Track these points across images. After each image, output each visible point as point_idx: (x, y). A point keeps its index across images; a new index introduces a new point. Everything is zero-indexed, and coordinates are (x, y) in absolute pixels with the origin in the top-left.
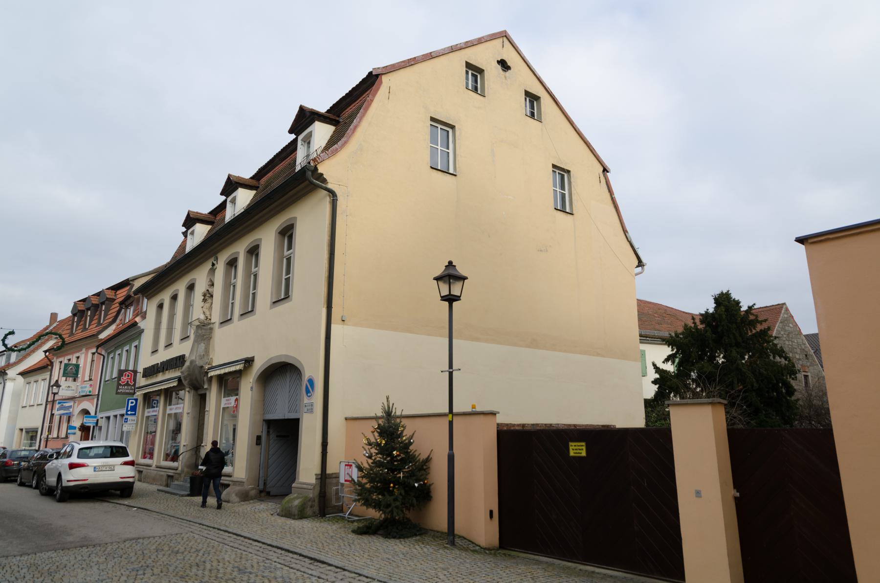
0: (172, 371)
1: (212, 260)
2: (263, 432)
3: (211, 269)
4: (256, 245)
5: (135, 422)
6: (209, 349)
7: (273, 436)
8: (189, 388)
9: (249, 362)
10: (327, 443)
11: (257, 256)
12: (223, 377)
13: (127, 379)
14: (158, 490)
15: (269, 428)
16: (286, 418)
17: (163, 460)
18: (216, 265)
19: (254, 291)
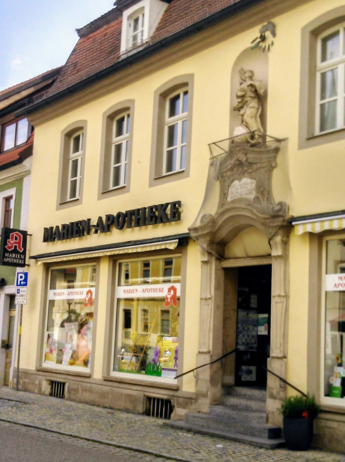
13: (15, 243)
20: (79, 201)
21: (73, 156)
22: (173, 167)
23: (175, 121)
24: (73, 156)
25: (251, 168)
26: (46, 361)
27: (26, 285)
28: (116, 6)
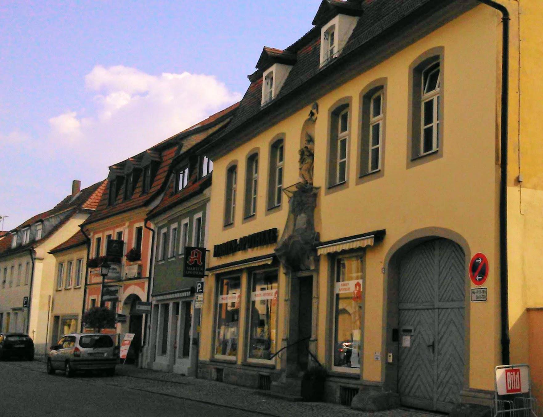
0: (257, 249)
1: (308, 109)
3: (308, 120)
9: (379, 236)
11: (282, 149)
13: (195, 258)
17: (180, 357)
18: (316, 115)
19: (343, 160)
20: (439, 153)
21: (374, 120)
23: (431, 97)
24: (426, 96)
25: (124, 266)
26: (218, 354)
27: (202, 292)
28: (258, 69)
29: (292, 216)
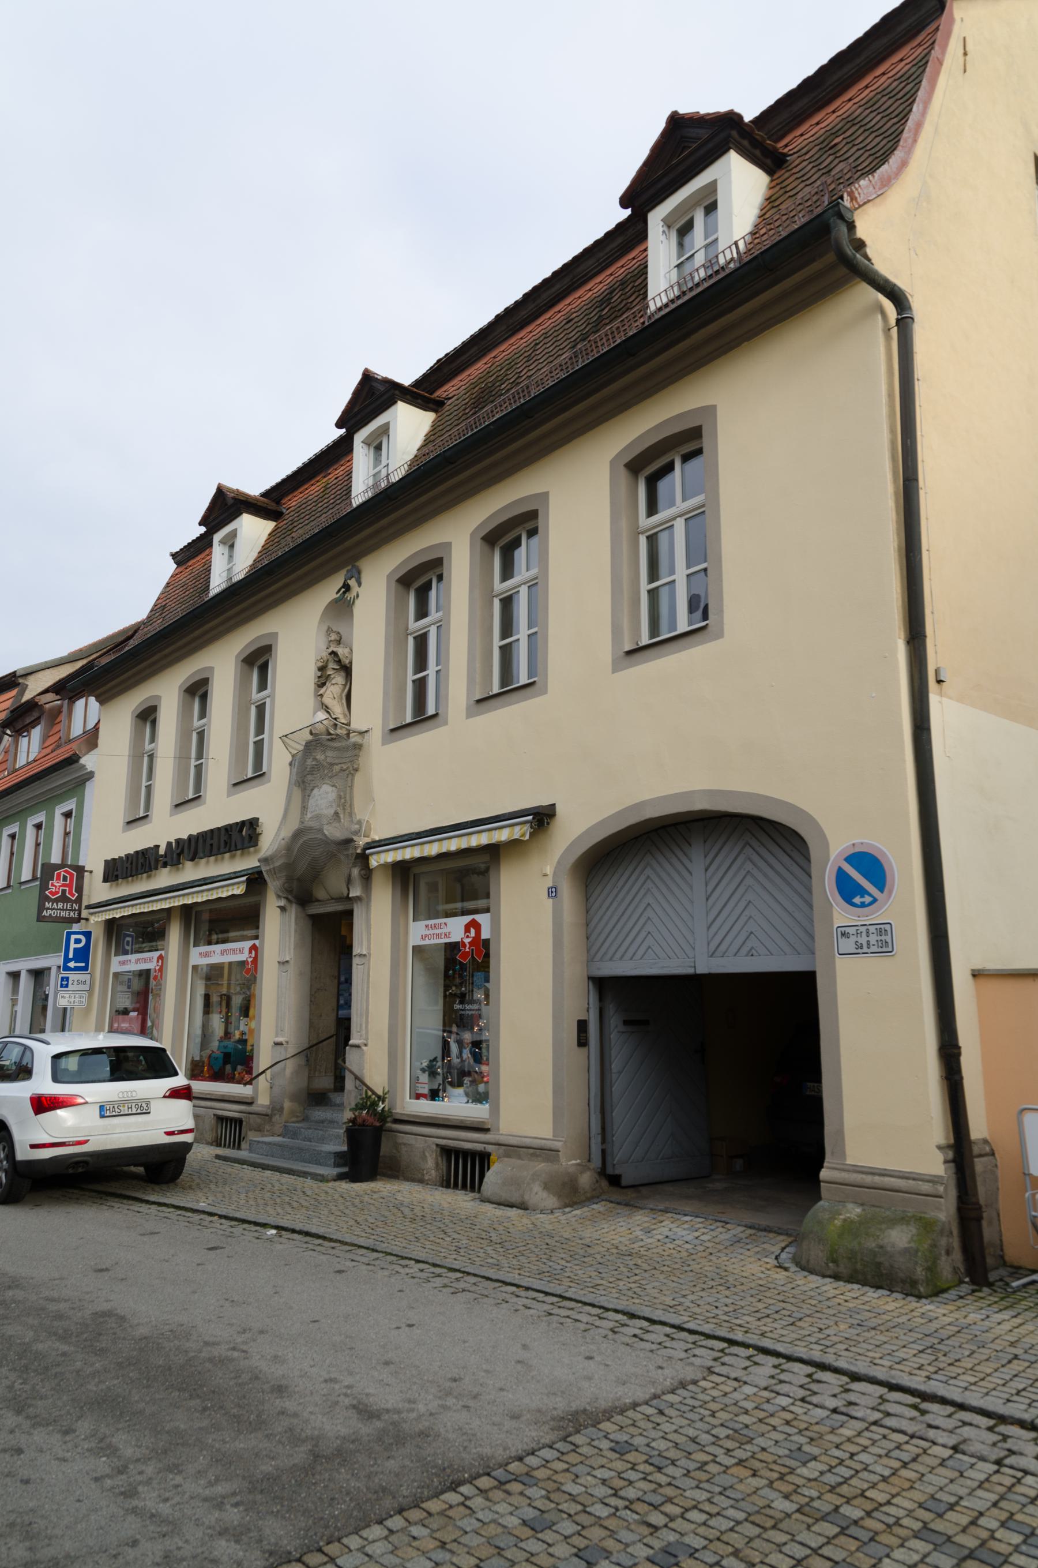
0: (208, 862)
1: (336, 582)
2: (591, 1011)
3: (335, 601)
4: (532, 511)
5: (87, 987)
6: (352, 798)
7: (614, 1021)
8: (287, 898)
10: (959, 1048)
11: (154, 723)
12: (409, 869)
13: (63, 885)
14: (218, 1157)
15: (601, 998)
16: (701, 970)
22: (515, 679)
23: (426, 627)
29: (297, 793)
